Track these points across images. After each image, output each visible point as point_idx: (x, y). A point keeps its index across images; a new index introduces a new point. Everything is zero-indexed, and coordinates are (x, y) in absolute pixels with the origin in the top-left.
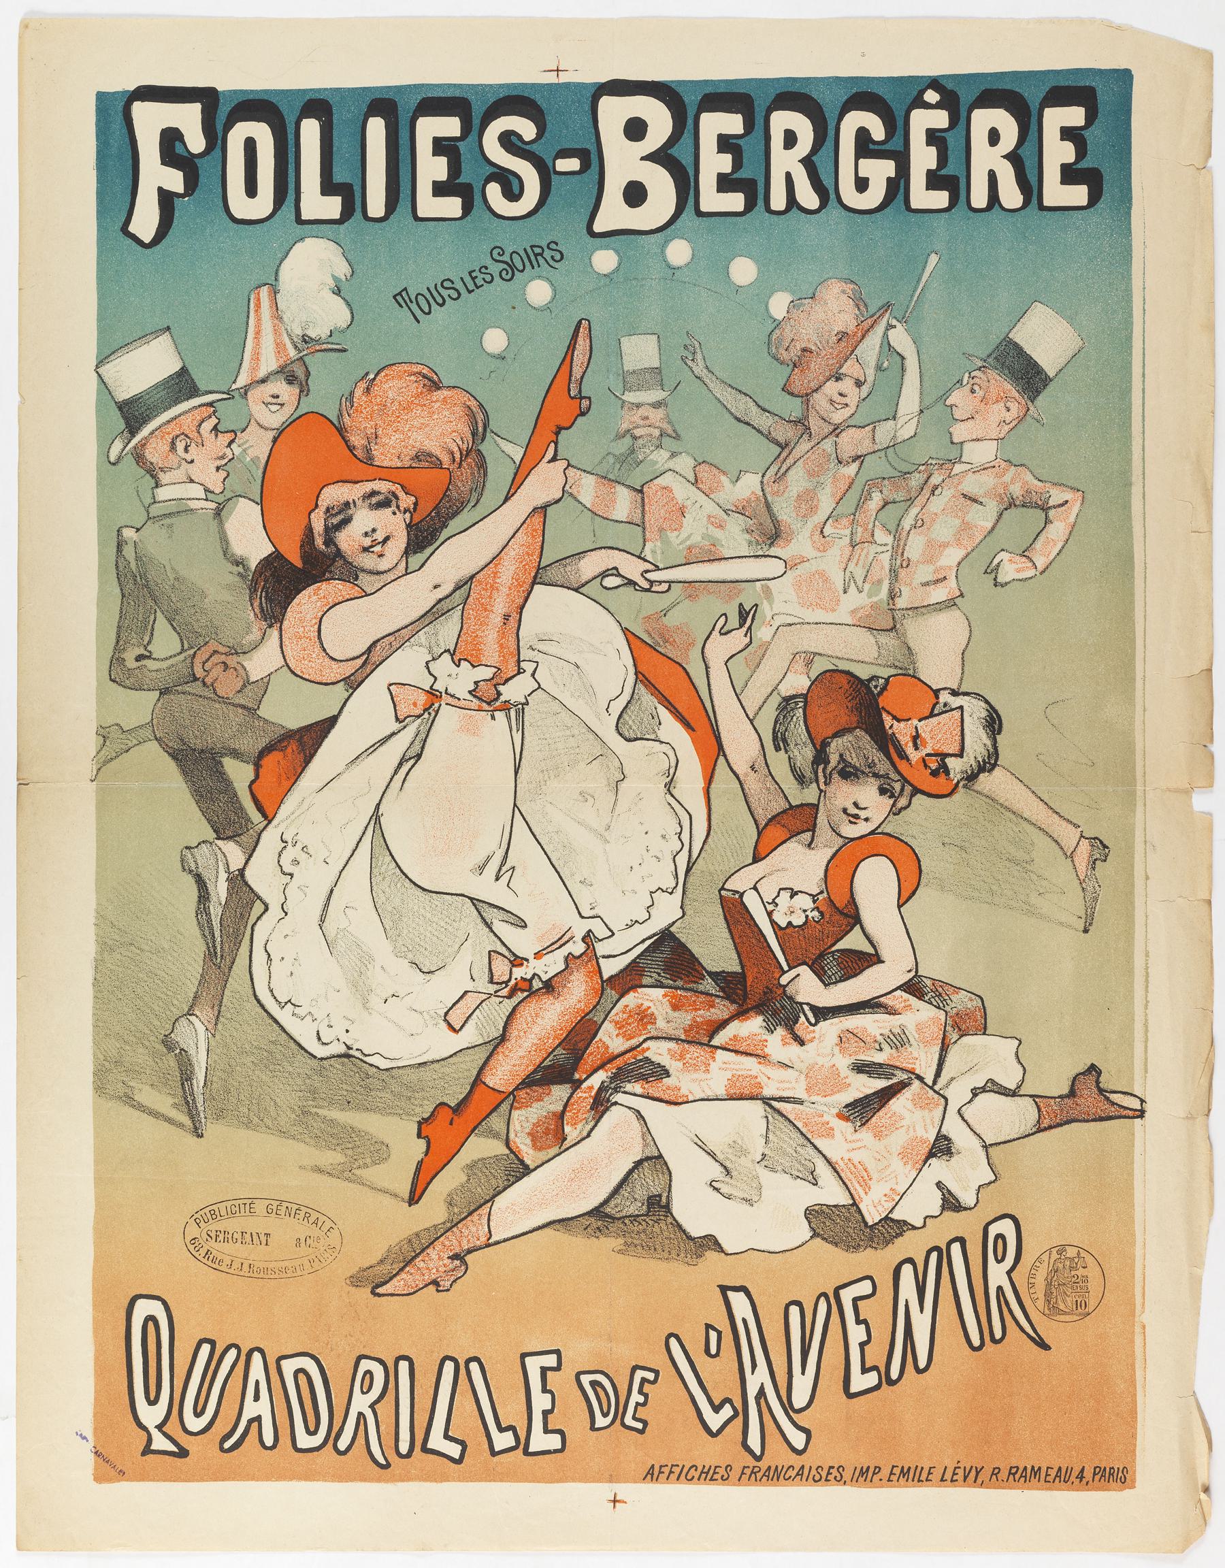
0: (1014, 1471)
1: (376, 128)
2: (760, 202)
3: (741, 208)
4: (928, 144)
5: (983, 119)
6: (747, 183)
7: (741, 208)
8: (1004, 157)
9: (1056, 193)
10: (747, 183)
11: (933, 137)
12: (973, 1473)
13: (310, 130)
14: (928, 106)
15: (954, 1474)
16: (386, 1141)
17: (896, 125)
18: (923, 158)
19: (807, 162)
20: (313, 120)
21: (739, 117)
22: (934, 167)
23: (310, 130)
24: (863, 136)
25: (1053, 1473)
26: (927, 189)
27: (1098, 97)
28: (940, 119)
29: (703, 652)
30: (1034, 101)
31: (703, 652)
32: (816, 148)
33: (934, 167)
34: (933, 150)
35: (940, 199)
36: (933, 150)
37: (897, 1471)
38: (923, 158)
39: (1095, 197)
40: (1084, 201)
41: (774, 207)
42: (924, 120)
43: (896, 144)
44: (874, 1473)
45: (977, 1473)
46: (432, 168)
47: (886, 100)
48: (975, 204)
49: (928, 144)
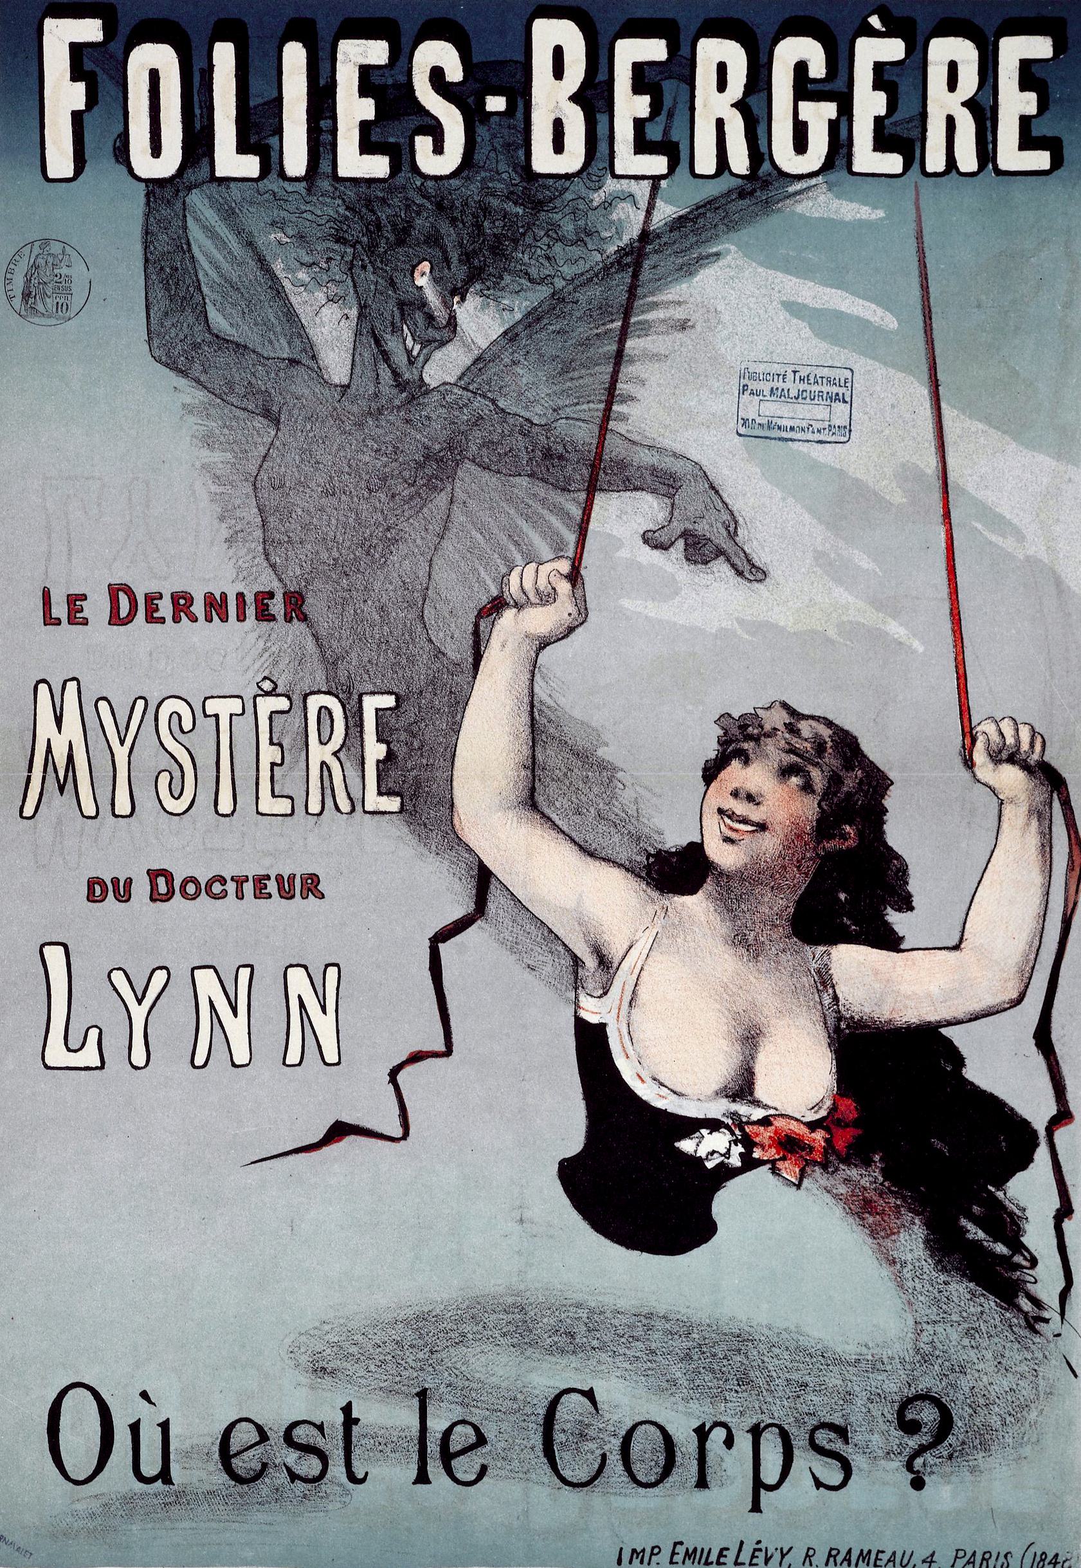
0: (834, 1553)
4: (74, 79)
6: (900, 135)
7: (1047, 167)
8: (732, 106)
9: (1010, 155)
10: (900, 135)
11: (883, 76)
12: (778, 1556)
13: (224, 55)
14: (872, 33)
15: (753, 1556)
16: (710, 1150)
18: (869, 104)
19: (741, 106)
21: (663, 42)
23: (224, 55)
24: (801, 68)
26: (875, 150)
32: (749, 89)
33: (883, 112)
34: (81, 87)
35: (893, 163)
36: (81, 87)
37: (681, 1550)
38: (869, 104)
43: (839, 85)
44: (652, 1554)
45: (783, 1556)
48: (699, 170)
49: (74, 79)
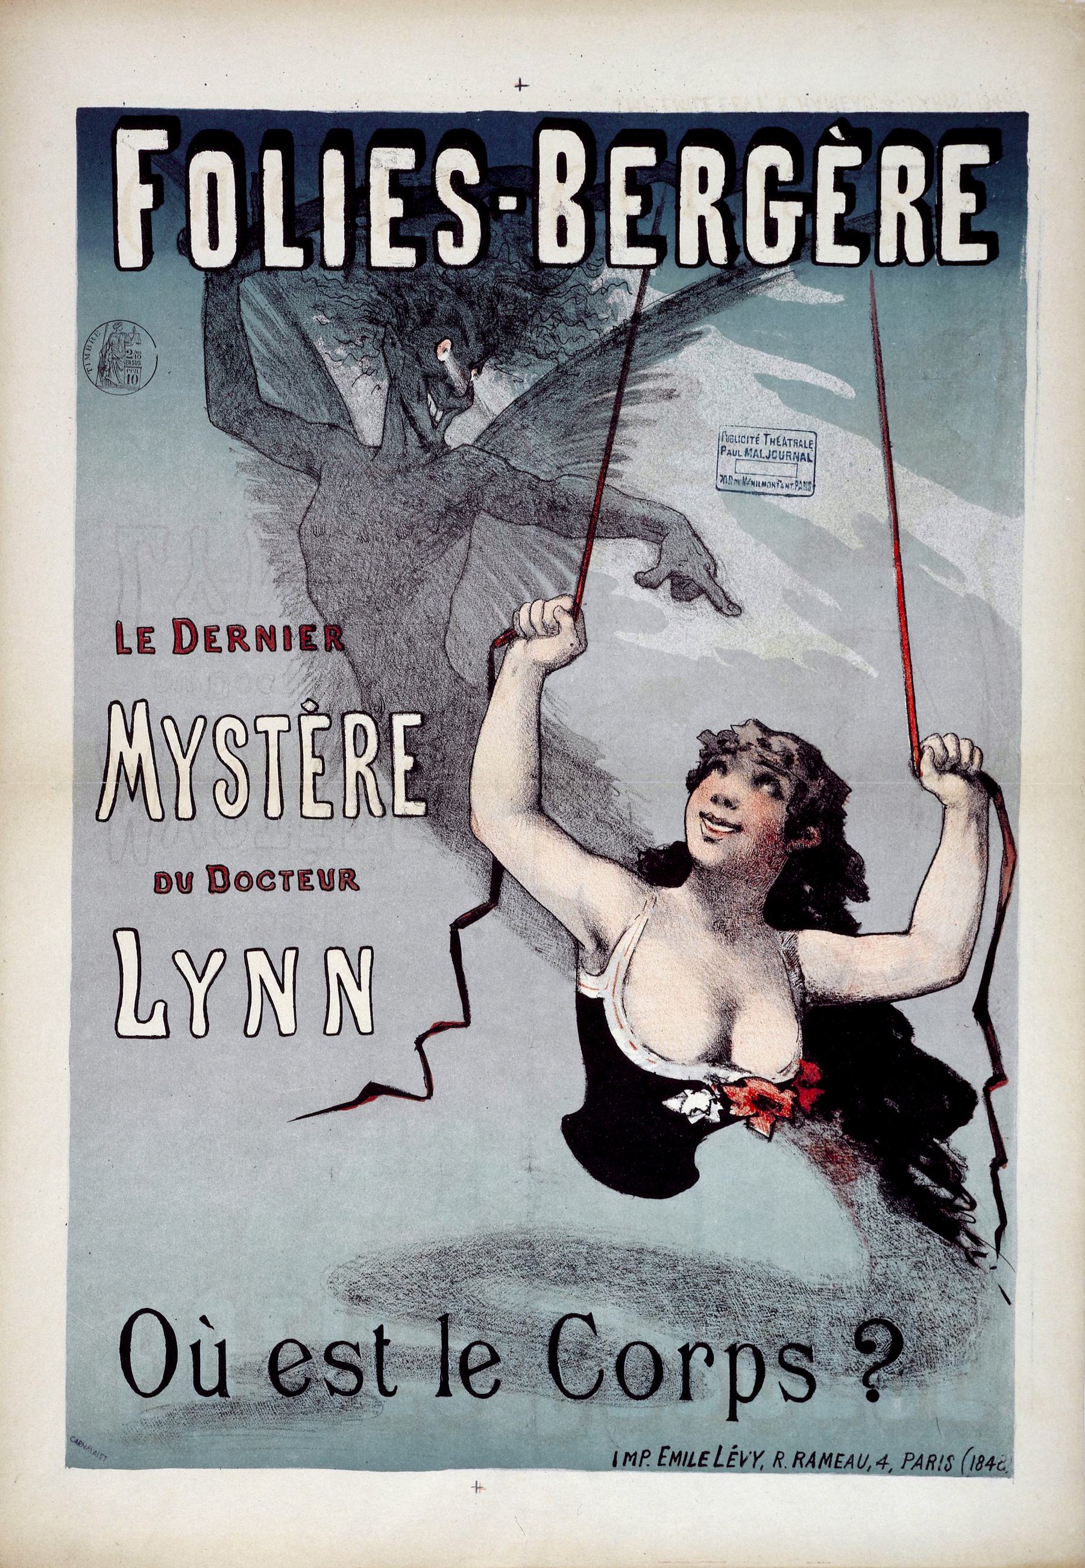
0: (800, 1456)
1: (334, 161)
2: (871, 257)
3: (857, 260)
4: (143, 181)
5: (894, 157)
7: (857, 260)
9: (952, 248)
11: (843, 179)
13: (273, 161)
15: (730, 1459)
17: (805, 166)
18: (831, 203)
19: (719, 205)
20: (857, 148)
21: (652, 150)
22: (842, 210)
23: (273, 161)
24: (772, 172)
25: (844, 1459)
27: (1003, 134)
28: (851, 156)
29: (239, 719)
30: (935, 139)
31: (239, 719)
32: (727, 190)
33: (842, 210)
34: (149, 189)
35: (851, 254)
36: (149, 189)
37: (668, 1453)
38: (831, 203)
39: (993, 253)
40: (984, 257)
41: (883, 260)
42: (833, 158)
43: (805, 187)
44: (643, 1457)
45: (756, 1458)
46: (385, 208)
47: (800, 133)
49: (143, 181)
